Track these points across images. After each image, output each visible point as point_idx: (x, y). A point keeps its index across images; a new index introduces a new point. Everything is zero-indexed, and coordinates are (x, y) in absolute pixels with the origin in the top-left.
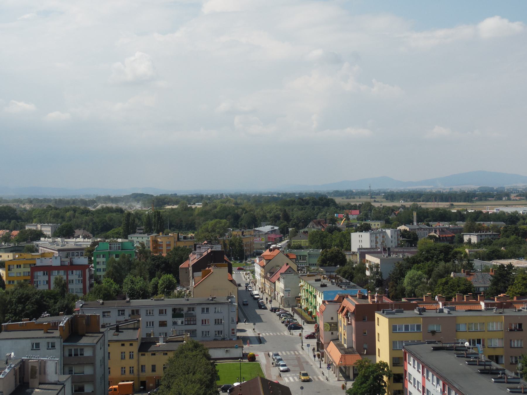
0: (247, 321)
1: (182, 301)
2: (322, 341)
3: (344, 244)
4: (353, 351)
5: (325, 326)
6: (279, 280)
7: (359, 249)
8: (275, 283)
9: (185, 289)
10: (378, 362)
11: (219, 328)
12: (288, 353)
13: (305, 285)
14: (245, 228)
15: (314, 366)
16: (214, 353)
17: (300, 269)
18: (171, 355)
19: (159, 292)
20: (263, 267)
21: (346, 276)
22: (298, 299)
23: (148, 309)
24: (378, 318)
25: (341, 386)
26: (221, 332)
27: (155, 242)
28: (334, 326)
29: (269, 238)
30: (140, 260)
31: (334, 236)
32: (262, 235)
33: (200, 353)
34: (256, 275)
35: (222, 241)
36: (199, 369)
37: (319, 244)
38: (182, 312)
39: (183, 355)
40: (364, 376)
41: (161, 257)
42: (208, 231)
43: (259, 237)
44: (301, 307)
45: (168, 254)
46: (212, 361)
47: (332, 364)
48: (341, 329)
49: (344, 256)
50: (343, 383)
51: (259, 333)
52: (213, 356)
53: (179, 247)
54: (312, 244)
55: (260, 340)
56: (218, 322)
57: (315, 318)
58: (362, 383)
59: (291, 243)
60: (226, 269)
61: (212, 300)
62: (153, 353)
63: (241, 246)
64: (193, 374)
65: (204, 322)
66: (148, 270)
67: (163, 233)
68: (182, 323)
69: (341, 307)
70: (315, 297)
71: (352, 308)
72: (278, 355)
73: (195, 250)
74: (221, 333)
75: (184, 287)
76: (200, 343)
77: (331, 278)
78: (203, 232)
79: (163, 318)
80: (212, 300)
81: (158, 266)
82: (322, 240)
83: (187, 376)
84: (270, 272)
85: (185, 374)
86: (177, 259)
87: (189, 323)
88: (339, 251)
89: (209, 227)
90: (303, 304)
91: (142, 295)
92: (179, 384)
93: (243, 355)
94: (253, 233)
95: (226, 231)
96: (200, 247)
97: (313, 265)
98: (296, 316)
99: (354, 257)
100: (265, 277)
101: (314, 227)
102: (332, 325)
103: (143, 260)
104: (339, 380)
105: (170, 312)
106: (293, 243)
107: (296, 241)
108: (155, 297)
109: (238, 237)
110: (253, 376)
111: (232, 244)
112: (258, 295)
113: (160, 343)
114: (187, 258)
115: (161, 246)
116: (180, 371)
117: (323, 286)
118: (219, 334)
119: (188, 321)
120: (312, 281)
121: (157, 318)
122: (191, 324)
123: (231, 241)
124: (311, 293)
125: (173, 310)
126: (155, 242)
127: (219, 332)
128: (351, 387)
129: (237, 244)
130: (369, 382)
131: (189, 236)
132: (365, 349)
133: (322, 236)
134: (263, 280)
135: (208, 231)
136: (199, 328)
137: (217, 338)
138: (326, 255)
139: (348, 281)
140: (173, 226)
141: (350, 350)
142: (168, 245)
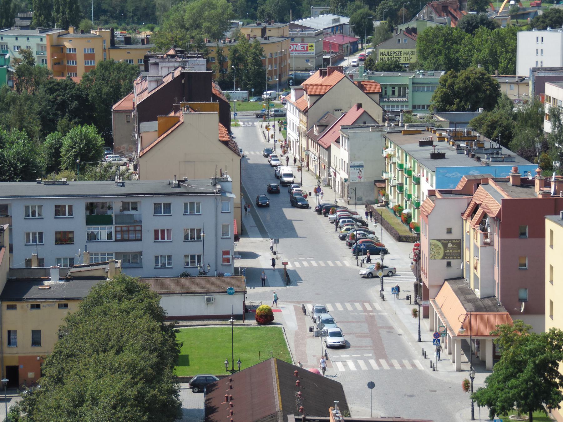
0: (263, 234)
1: (110, 187)
2: (426, 281)
3: (502, 59)
4: (495, 305)
5: (432, 247)
6: (338, 141)
7: (534, 70)
8: (329, 149)
9: (125, 160)
10: (547, 331)
11: (194, 248)
12: (349, 306)
13: (398, 153)
14: (270, 19)
15: (405, 338)
16: (171, 306)
17: (393, 113)
18: (74, 308)
19: (63, 166)
20: (305, 112)
21: (496, 132)
22: (380, 185)
23: (30, 204)
24: (552, 232)
25: (461, 382)
26: (199, 257)
27: (58, 48)
28: (453, 249)
29: (326, 44)
30: (19, 91)
31: (476, 40)
32: (310, 36)
33: (139, 305)
34: (289, 130)
35: (215, 50)
36: (131, 341)
37: (441, 59)
38: (109, 213)
39: (97, 309)
40: (513, 362)
41: (68, 86)
42: (183, 26)
43: (303, 41)
44: (387, 204)
45: (86, 78)
46: (167, 323)
47: (445, 333)
48: (469, 255)
49: (495, 88)
50: (466, 376)
51: (285, 260)
52: (170, 312)
53: (112, 63)
54: (425, 58)
55: (287, 275)
56: (193, 236)
57: (417, 229)
58: (507, 379)
59: (376, 55)
60: (215, 116)
61: (179, 186)
62: (35, 303)
63: (259, 63)
64: (118, 353)
65: (160, 235)
66: (40, 113)
67: (77, 28)
68: (109, 236)
69: (472, 205)
70: (418, 182)
71: (495, 208)
72: (323, 310)
73: (147, 70)
74: (199, 261)
75: (122, 155)
76: (140, 283)
77: (456, 137)
78: (171, 28)
79: (64, 225)
80: (179, 186)
81: (62, 106)
82: (448, 48)
83: (102, 355)
84: (320, 125)
85: (97, 351)
86: (105, 90)
87: (126, 236)
88: (483, 74)
89: (187, 16)
90: (391, 197)
91: (22, 171)
92: (83, 373)
93: (247, 309)
94: (287, 33)
95: (225, 25)
96: (156, 64)
97: (423, 107)
98: (372, 225)
99: (522, 88)
100: (309, 136)
101: (431, 19)
102: (450, 245)
103: (27, 91)
104: (459, 370)
105: (80, 212)
106: (380, 57)
107: (386, 52)
108: (53, 177)
109: (252, 41)
110: (265, 356)
111: (238, 59)
112: (290, 175)
113: (53, 281)
114: (130, 90)
115: (72, 58)
116: (88, 345)
117: (436, 156)
118: (193, 262)
119: (122, 231)
120: (412, 143)
121: (50, 225)
122: (128, 240)
123: (235, 51)
124: (409, 173)
125: (87, 208)
126: (58, 48)
127: (193, 257)
128: (484, 386)
129: (250, 59)
130: (524, 376)
131: (143, 35)
132: (521, 300)
133: (450, 40)
134: (304, 142)
135: (183, 26)
136: (148, 248)
137: (190, 271)
138: (452, 86)
139: (495, 145)
140: (105, 12)
141: (488, 302)
142: (89, 57)
